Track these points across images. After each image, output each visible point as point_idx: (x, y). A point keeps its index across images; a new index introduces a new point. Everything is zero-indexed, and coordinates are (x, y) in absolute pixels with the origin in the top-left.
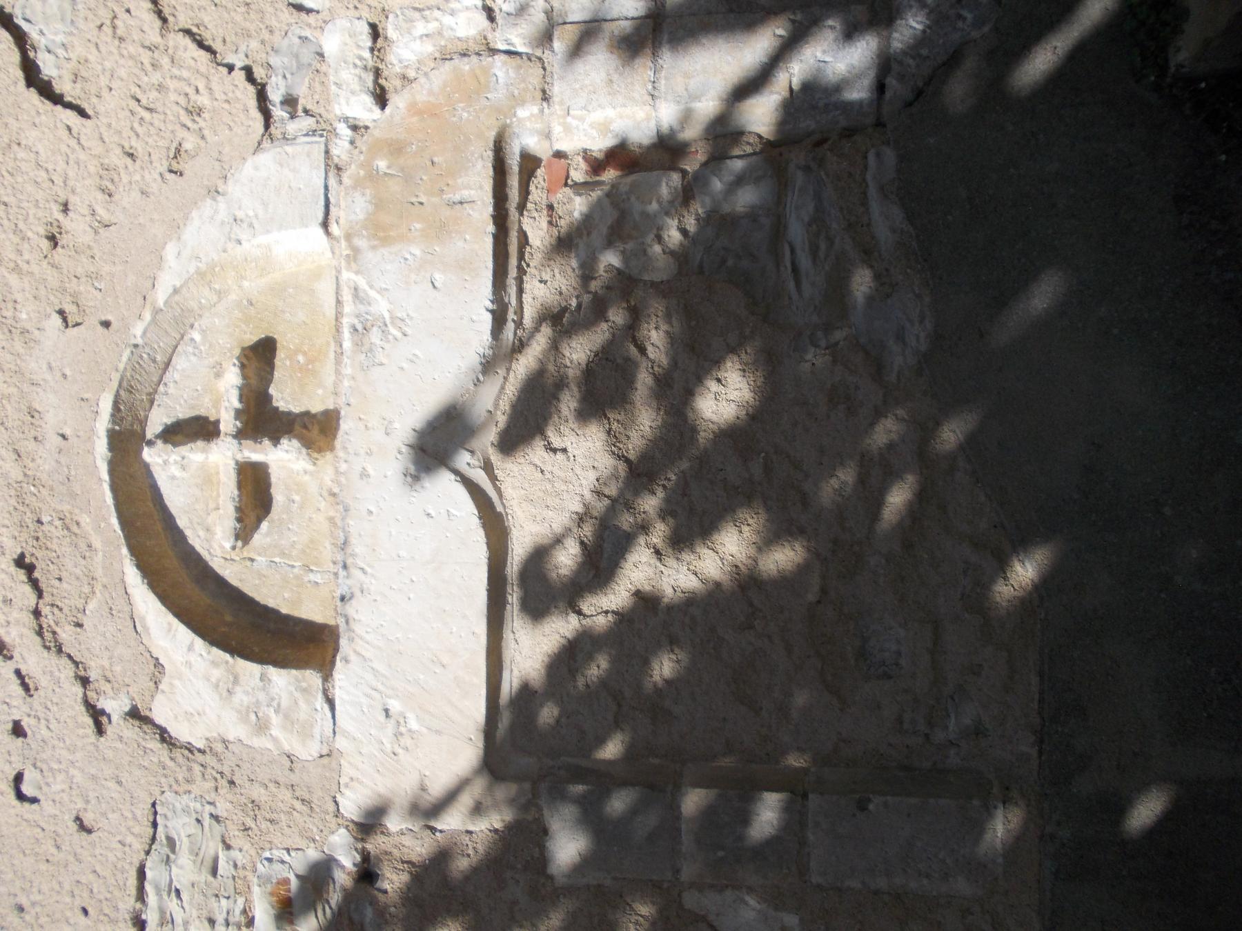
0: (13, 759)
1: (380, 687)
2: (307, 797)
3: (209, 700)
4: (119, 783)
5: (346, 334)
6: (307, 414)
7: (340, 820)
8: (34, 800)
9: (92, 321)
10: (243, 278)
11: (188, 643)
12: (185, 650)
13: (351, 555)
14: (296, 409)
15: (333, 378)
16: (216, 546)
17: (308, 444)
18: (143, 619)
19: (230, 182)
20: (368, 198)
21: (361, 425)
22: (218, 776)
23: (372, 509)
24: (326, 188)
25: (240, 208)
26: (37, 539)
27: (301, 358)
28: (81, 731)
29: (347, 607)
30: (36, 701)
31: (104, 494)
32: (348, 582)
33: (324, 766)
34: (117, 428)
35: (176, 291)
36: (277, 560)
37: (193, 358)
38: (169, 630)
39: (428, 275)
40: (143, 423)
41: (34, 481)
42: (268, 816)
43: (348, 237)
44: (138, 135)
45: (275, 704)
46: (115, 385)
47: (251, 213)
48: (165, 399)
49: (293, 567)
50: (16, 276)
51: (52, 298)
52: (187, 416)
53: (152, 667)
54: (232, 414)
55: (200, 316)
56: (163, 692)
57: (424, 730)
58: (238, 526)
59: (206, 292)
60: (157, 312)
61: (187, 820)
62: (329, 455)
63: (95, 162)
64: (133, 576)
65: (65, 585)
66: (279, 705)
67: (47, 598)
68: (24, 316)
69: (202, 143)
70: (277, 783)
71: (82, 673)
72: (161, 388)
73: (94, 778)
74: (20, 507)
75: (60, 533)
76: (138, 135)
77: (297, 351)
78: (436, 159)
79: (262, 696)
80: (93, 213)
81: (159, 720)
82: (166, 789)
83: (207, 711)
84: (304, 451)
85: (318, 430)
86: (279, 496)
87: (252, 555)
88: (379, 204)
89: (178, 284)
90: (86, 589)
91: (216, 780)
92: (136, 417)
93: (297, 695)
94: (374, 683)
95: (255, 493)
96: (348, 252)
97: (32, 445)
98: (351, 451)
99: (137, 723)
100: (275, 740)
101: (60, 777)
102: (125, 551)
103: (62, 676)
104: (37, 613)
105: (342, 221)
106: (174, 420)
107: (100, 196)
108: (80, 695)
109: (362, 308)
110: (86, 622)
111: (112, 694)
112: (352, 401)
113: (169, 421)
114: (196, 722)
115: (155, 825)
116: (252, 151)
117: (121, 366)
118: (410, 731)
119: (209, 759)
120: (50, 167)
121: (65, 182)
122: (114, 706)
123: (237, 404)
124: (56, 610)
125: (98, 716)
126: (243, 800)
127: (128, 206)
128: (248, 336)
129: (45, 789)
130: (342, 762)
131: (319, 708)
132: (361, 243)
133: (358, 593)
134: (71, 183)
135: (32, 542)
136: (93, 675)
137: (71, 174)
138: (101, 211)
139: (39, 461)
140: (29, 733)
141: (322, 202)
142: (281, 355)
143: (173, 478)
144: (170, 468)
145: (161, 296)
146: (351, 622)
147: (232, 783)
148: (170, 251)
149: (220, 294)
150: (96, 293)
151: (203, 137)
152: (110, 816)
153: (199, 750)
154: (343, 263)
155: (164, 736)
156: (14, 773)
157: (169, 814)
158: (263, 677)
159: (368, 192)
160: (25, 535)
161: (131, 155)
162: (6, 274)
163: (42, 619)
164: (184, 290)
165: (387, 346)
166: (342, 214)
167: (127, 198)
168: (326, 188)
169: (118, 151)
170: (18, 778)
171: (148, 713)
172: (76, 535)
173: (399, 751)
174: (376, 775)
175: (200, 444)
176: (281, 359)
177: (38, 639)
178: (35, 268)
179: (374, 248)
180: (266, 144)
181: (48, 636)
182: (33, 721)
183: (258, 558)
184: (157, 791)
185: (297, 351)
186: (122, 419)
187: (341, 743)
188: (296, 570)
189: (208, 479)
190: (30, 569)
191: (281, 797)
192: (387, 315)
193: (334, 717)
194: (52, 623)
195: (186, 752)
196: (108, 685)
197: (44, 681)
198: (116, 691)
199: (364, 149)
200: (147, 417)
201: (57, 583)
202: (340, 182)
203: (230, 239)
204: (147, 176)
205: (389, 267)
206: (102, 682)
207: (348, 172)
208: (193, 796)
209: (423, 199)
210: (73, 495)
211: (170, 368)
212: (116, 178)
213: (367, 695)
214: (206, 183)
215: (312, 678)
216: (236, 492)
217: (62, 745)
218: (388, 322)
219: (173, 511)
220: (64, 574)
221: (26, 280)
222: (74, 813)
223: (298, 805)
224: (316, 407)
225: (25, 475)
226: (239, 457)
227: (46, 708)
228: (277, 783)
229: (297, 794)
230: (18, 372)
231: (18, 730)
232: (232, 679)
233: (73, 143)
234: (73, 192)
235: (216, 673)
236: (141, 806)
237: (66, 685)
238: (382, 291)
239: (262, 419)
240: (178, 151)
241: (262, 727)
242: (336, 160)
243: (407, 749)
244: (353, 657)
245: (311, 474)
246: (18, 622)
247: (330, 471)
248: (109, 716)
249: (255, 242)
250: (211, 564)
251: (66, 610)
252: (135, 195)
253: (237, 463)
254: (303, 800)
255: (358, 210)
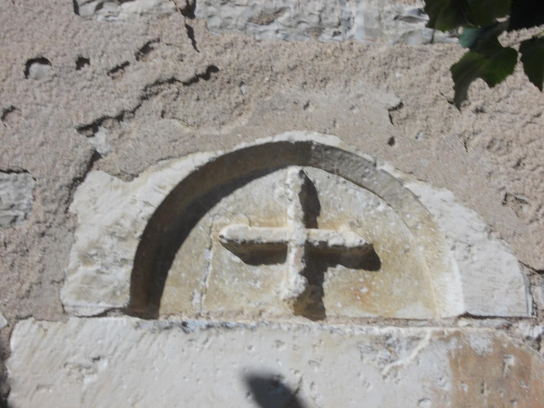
0: (60, 58)
1: (117, 354)
2: (32, 294)
3: (107, 218)
4: (42, 144)
5: (386, 330)
6: (322, 294)
7: (13, 320)
8: (27, 73)
9: (394, 132)
10: (426, 247)
11: (151, 202)
12: (145, 200)
13: (218, 332)
14: (326, 285)
15: (350, 315)
16: (222, 220)
17: (301, 298)
18: (168, 166)
19: (498, 242)
20: (487, 350)
21: (316, 342)
22: (48, 224)
23: (253, 349)
24: (494, 317)
25: (479, 250)
26: (229, 82)
27: (365, 290)
28: (81, 114)
29: (179, 329)
30: (103, 78)
31: (263, 137)
32: (197, 330)
33: (55, 308)
34: (313, 148)
35: (416, 198)
36: (211, 268)
37: (365, 204)
38: (160, 187)
39: (429, 397)
40: (316, 165)
41: (273, 80)
42: (16, 262)
43: (457, 334)
44: (533, 170)
45: (104, 270)
46: (346, 148)
47: (475, 258)
48: (334, 182)
49: (205, 280)
50: (428, 69)
51: (411, 98)
52: (320, 200)
53: (132, 172)
54: (324, 239)
55: (397, 212)
56: (112, 180)
57: (84, 388)
58: (239, 242)
59: (416, 219)
60: (401, 182)
61: (13, 197)
62: (291, 311)
63: (513, 135)
64: (202, 158)
65: (193, 103)
66: (103, 273)
67: (183, 89)
68: (398, 75)
69: (527, 221)
70: (43, 270)
71: (126, 116)
72: (342, 179)
73: (46, 124)
74: (252, 70)
75: (233, 101)
76: (533, 170)
77: (370, 287)
78: (515, 403)
79: (109, 259)
80: (474, 134)
81: (90, 177)
82: (38, 182)
83: (99, 216)
84: (296, 295)
85: (310, 304)
86: (259, 270)
87: (214, 248)
88: (482, 358)
89: (422, 200)
90: (190, 120)
91: (45, 222)
92: (321, 160)
93: (111, 287)
94: (120, 349)
95: (263, 254)
96: (446, 333)
97: (300, 79)
98: (297, 333)
99: (88, 159)
100: (76, 269)
101: (46, 98)
102: (220, 153)
103: (124, 100)
104: (172, 81)
105: (469, 328)
106: (318, 190)
107: (488, 139)
108: (110, 114)
109: (404, 343)
110: (166, 120)
111: (110, 139)
112: (335, 335)
113: (317, 186)
114: (89, 206)
115: (9, 171)
116: (522, 260)
117: (360, 154)
118: (83, 377)
119: (61, 216)
120: (510, 100)
121: (499, 111)
122: (101, 140)
123: (331, 243)
124: (174, 96)
125: (93, 128)
126: (29, 243)
127: (480, 161)
128: (381, 248)
129: (37, 82)
130: (59, 323)
131: (101, 304)
132: (454, 341)
133: (189, 337)
134: (498, 116)
135: (226, 78)
136: (124, 124)
137: (505, 116)
138: (477, 139)
139: (288, 85)
140: (80, 72)
141: (483, 314)
142: (367, 274)
143: (274, 187)
144: (286, 181)
145: (413, 186)
146: (167, 331)
147: (43, 234)
148: (446, 194)
149: (414, 229)
150: (415, 134)
151: (531, 221)
152: (16, 136)
153: (67, 209)
154: (438, 329)
155: (79, 180)
156: (49, 59)
157: (17, 183)
158: (124, 261)
159: (491, 350)
160: (231, 72)
161: (518, 164)
162: (429, 62)
163: (167, 85)
164: (417, 204)
165: (376, 363)
166: (475, 329)
167: (486, 160)
168: (494, 317)
169: (521, 154)
170: (43, 61)
171: (95, 166)
172: (232, 113)
173: (68, 369)
174: (48, 350)
175: (301, 214)
176: (364, 275)
177: (152, 81)
178: (434, 85)
179: (450, 354)
180: (527, 271)
181: (154, 89)
182: (89, 75)
183: (211, 253)
184: (36, 174)
185: (370, 287)
186: (320, 152)
187: (73, 322)
188: (202, 283)
189: (273, 217)
190: (206, 76)
191: (32, 273)
192: (399, 363)
193: (94, 316)
194: (165, 92)
195: (66, 198)
196: (116, 136)
197: (120, 84)
198: (113, 143)
199: (523, 348)
200: (320, 167)
201: (195, 97)
202: (498, 328)
203: (456, 241)
204: (502, 177)
205: (435, 365)
206: (119, 131)
207: (505, 335)
208: (32, 202)
209: (486, 393)
210: (262, 112)
211: (357, 187)
212: (502, 151)
213: (110, 344)
214: (497, 223)
215: (124, 300)
216: (265, 241)
217: (71, 98)
218: (394, 364)
219: (248, 186)
220: (201, 103)
221: (425, 77)
222: (18, 107)
223: (26, 287)
224: (327, 302)
225: (277, 73)
226: (291, 244)
227: (100, 86)
228: (43, 270)
229: (34, 287)
230: (355, 71)
231: (81, 62)
232: (123, 235)
233: (528, 118)
234: (491, 118)
235: (127, 224)
236: (24, 162)
237: (117, 103)
238: (417, 359)
239: (319, 260)
240: (522, 201)
241: (86, 259)
242: (515, 325)
243: (69, 374)
244: (140, 332)
245: (277, 297)
246: (166, 65)
247: (279, 312)
248: (93, 136)
249: (453, 261)
250: (207, 215)
251: (174, 104)
252: (489, 167)
253: (287, 242)
254: (29, 291)
255: (477, 342)
